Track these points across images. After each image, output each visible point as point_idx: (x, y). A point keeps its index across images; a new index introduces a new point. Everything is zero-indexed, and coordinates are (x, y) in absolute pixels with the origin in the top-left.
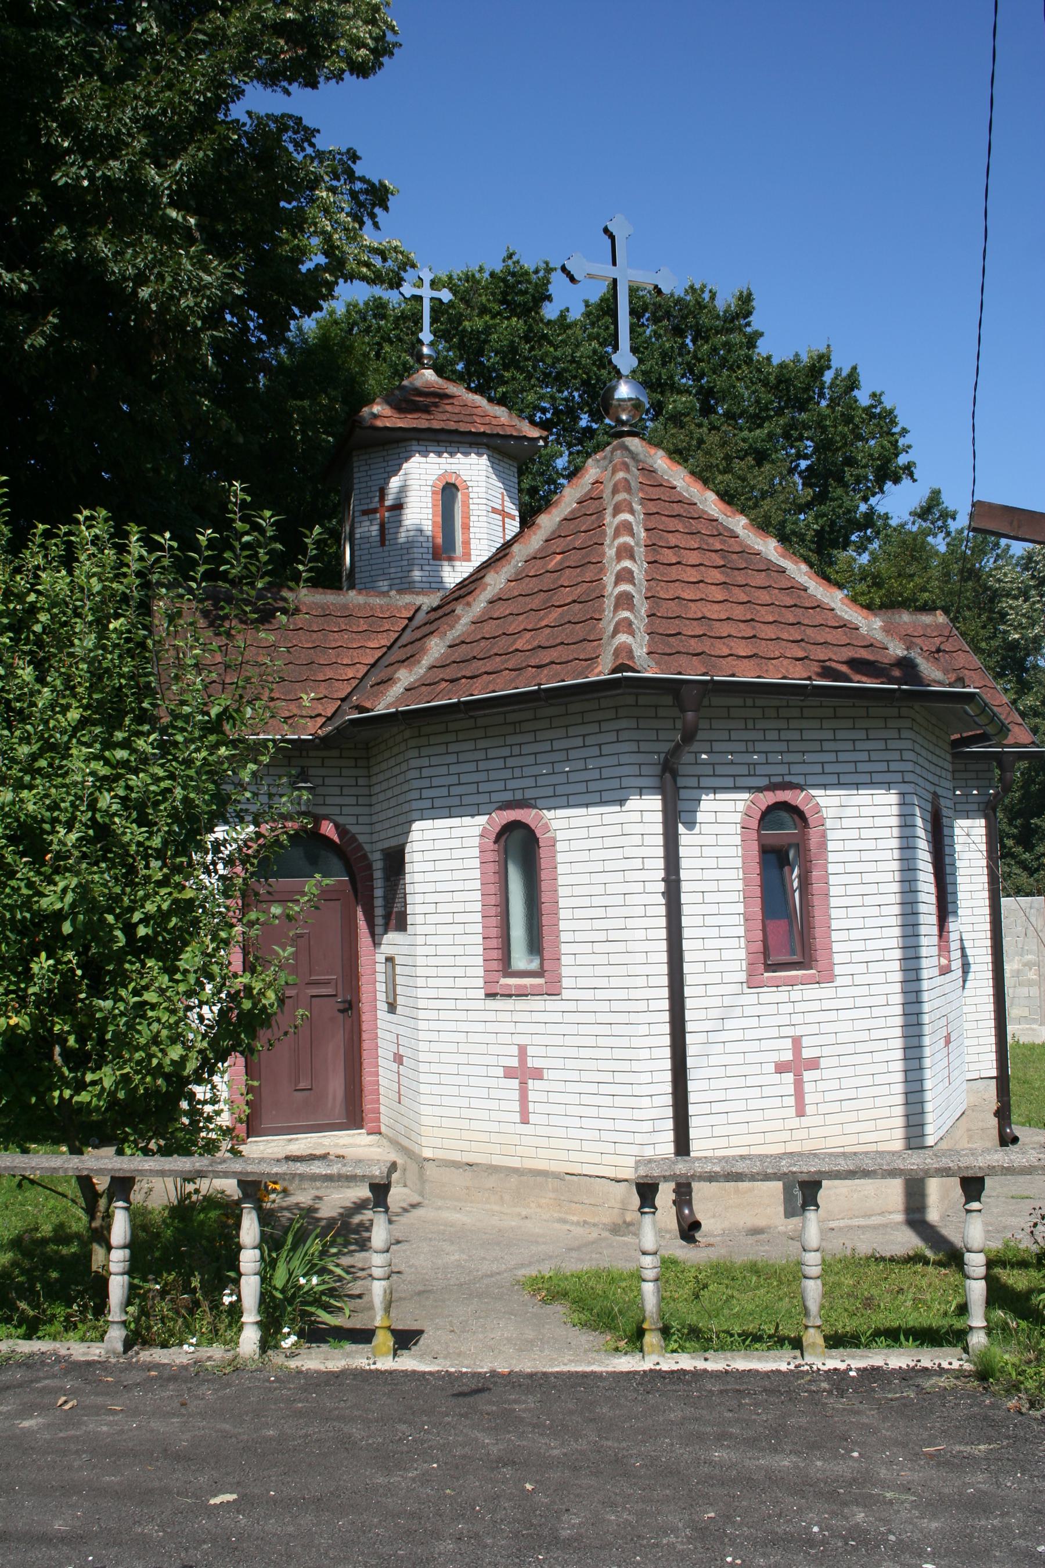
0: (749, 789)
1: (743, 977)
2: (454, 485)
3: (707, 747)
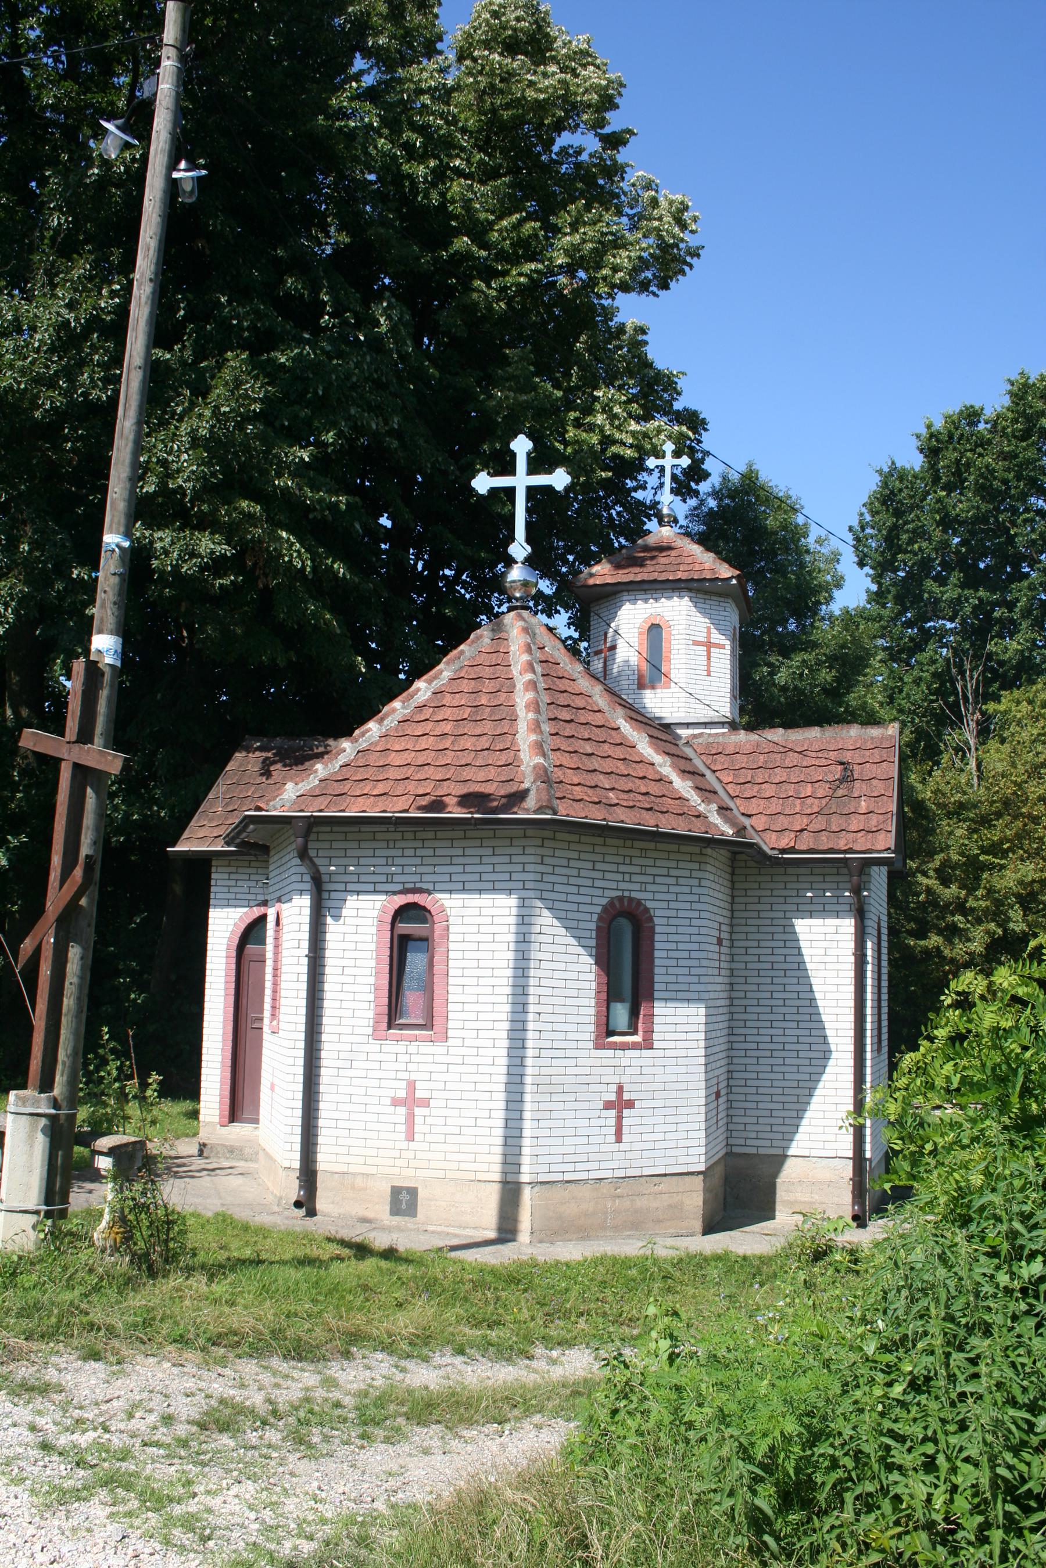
0: (387, 892)
1: (370, 1031)
2: (658, 626)
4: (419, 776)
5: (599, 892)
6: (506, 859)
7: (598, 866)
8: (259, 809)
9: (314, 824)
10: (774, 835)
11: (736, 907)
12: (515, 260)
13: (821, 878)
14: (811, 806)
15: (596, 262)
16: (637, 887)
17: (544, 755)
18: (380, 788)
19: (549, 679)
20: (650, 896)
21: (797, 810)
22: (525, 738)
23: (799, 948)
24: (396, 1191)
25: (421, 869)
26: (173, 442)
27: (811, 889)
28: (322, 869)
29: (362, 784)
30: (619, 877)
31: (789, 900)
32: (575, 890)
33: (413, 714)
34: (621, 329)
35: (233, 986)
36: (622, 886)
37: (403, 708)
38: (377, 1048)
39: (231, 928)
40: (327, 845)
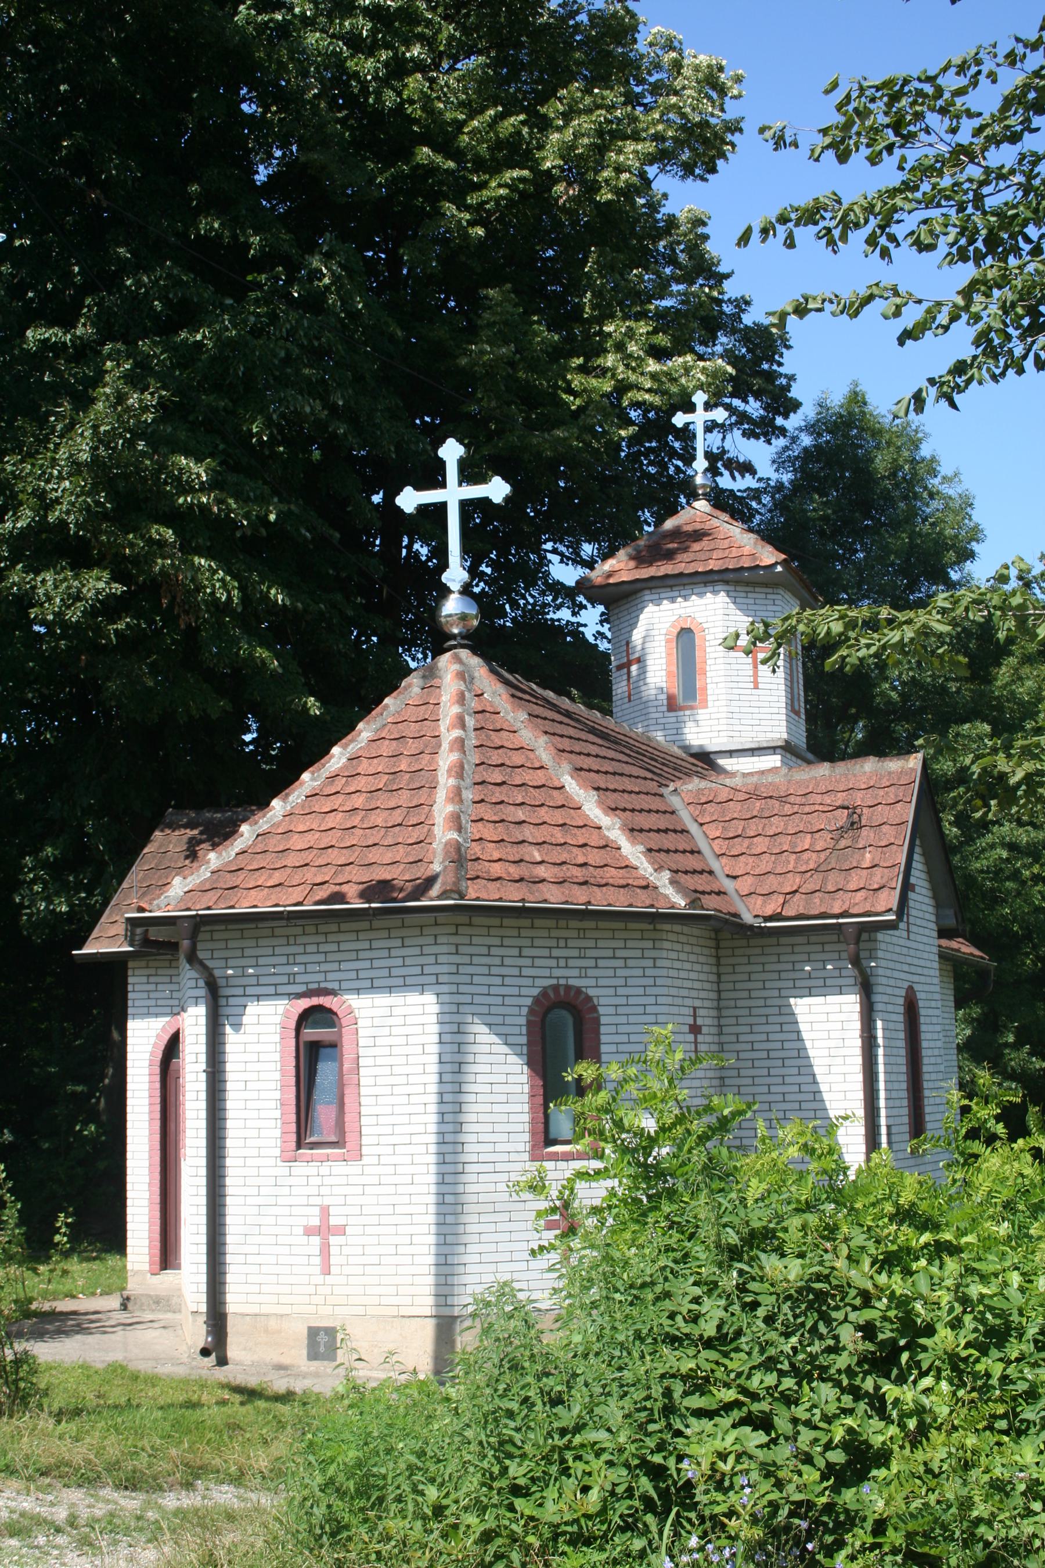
3: (253, 961)
4: (321, 861)
5: (529, 982)
6: (417, 950)
7: (526, 952)
8: (141, 909)
9: (200, 923)
10: (760, 900)
11: (723, 986)
12: (495, 168)
13: (819, 948)
14: (807, 863)
15: (596, 161)
16: (575, 972)
17: (460, 829)
18: (277, 877)
19: (483, 734)
20: (592, 982)
21: (791, 867)
22: (442, 809)
23: (799, 1032)
24: (313, 1333)
25: (325, 967)
26: (53, 467)
27: (809, 961)
28: (217, 973)
29: (257, 873)
30: (553, 963)
31: (784, 975)
32: (498, 981)
33: (323, 785)
34: (672, 222)
35: (158, 1108)
36: (557, 973)
37: (313, 779)
38: (286, 1171)
39: (153, 1040)
40: (222, 945)
